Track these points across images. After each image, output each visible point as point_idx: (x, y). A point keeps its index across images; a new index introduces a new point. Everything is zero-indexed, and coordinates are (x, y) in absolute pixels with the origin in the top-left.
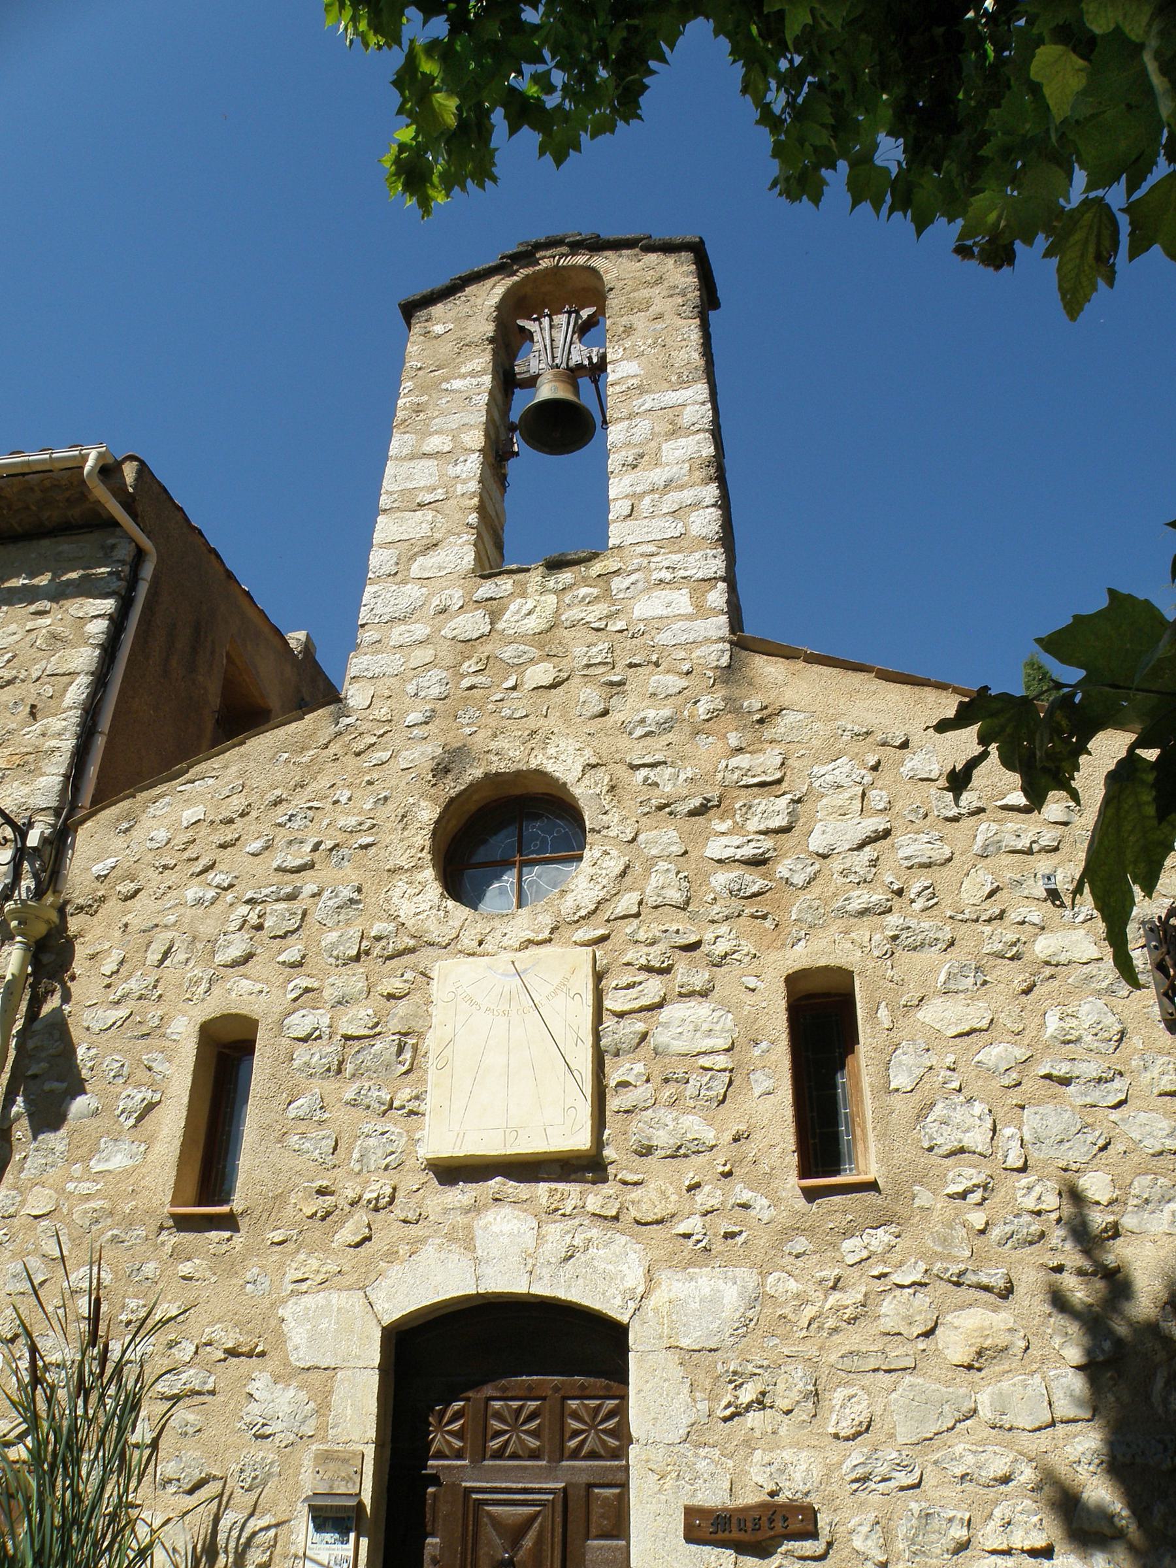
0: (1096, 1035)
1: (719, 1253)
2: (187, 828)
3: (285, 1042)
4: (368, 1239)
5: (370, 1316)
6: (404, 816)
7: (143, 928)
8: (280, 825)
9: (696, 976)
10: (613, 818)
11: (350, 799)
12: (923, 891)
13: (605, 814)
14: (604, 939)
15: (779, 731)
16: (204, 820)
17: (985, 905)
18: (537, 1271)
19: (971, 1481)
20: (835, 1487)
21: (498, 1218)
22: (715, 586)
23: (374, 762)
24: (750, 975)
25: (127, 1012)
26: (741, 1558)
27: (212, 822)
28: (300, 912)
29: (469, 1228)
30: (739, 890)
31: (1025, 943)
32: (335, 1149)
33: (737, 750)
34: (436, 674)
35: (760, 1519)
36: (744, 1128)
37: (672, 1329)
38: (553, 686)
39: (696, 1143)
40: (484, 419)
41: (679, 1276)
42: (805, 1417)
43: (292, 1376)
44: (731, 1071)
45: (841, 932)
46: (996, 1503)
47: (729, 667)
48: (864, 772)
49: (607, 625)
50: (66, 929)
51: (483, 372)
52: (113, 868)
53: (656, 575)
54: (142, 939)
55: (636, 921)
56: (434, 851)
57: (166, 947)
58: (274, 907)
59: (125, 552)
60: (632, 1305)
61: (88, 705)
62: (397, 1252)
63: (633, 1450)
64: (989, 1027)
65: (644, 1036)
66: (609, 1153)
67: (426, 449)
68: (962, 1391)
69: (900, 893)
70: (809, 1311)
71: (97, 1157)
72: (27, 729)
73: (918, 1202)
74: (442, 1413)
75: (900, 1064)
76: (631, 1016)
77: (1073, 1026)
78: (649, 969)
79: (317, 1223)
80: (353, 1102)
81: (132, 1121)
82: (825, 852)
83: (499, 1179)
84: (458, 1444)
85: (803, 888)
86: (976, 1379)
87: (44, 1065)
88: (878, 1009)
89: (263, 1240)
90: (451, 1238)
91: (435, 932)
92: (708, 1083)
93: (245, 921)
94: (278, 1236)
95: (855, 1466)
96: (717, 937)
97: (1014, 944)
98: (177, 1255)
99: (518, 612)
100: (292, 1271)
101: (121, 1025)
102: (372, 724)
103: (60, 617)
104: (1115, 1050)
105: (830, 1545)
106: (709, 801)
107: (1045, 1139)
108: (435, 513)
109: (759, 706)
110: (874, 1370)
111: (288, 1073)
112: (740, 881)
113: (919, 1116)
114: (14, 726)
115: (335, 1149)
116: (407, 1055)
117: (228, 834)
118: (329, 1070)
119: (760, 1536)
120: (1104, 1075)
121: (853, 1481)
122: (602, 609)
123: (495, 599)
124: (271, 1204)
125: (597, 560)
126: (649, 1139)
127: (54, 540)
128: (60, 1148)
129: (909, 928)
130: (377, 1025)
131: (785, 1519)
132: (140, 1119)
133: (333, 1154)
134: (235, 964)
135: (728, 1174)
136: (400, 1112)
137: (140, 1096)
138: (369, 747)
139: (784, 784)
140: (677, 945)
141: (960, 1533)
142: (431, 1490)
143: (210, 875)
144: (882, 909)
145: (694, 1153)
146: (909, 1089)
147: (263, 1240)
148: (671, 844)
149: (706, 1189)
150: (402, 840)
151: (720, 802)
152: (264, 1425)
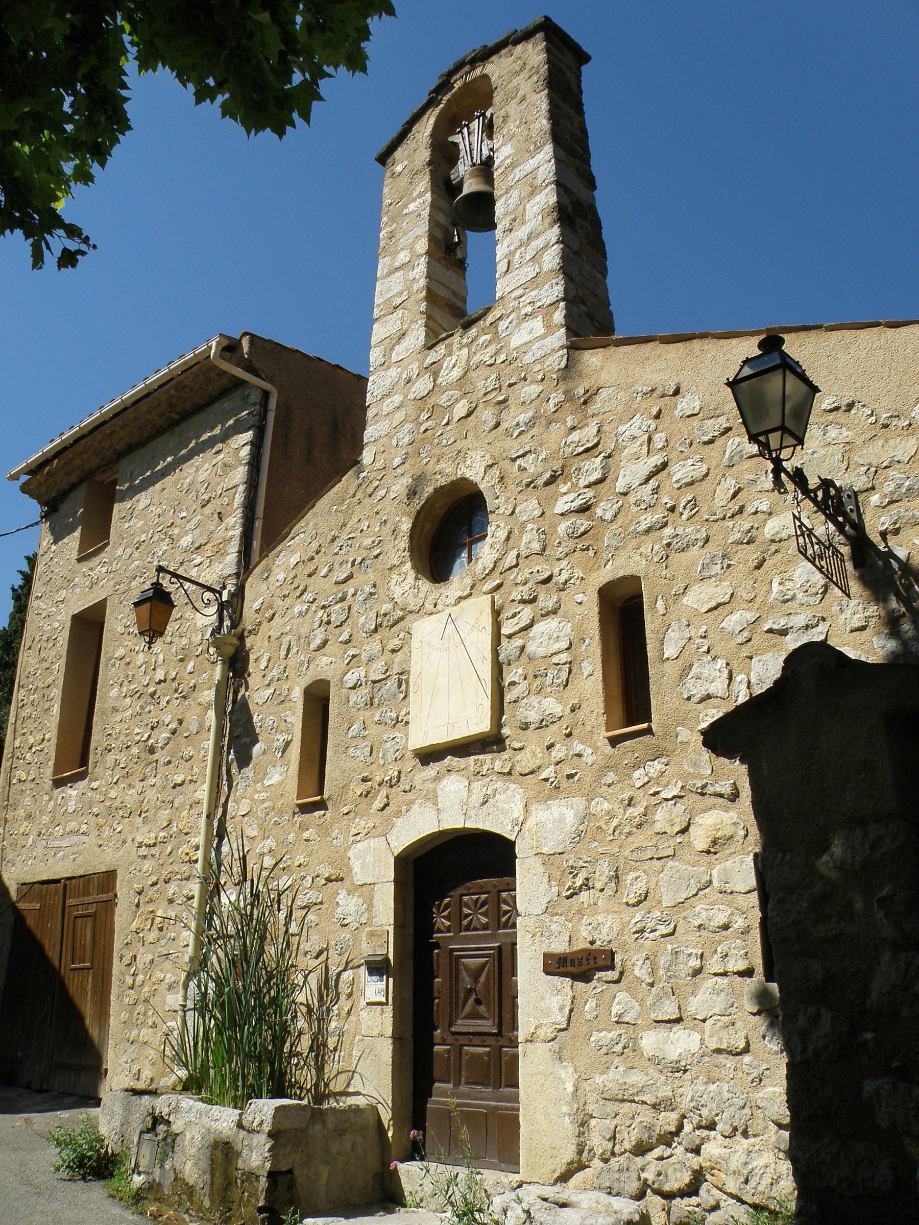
0: (807, 591)
1: (565, 789)
4: (387, 805)
5: (389, 851)
6: (394, 531)
8: (336, 554)
9: (546, 601)
10: (502, 500)
11: (368, 527)
12: (687, 504)
14: (499, 586)
18: (468, 814)
19: (704, 929)
20: (626, 937)
23: (378, 498)
26: (575, 983)
27: (304, 561)
29: (435, 790)
30: (573, 533)
31: (757, 528)
32: (371, 753)
34: (408, 426)
35: (582, 959)
36: (576, 702)
37: (538, 842)
38: (469, 415)
42: (611, 893)
43: (356, 890)
44: (570, 663)
46: (720, 942)
47: (566, 367)
48: (650, 422)
49: (495, 360)
51: (425, 192)
52: (262, 603)
53: (523, 312)
55: (517, 570)
56: (412, 549)
59: (255, 397)
60: (517, 829)
63: (519, 920)
65: (523, 648)
66: (506, 731)
67: (397, 264)
68: (702, 869)
69: (672, 509)
70: (615, 822)
73: (680, 739)
74: (439, 905)
75: (671, 639)
77: (790, 587)
78: (523, 602)
81: (280, 753)
83: (449, 757)
84: (448, 923)
85: (612, 521)
86: (713, 860)
87: (241, 729)
88: (656, 601)
95: (636, 923)
96: (561, 570)
97: (749, 531)
98: (303, 828)
99: (447, 368)
104: (821, 601)
105: (622, 973)
106: (556, 472)
107: (765, 679)
109: (582, 392)
110: (651, 859)
113: (682, 676)
114: (213, 528)
115: (371, 753)
116: (404, 687)
117: (311, 567)
118: (366, 704)
119: (582, 969)
120: (810, 622)
121: (634, 933)
122: (492, 348)
123: (435, 363)
126: (526, 718)
128: (251, 775)
129: (678, 535)
130: (387, 670)
131: (595, 958)
132: (284, 752)
134: (319, 648)
135: (569, 735)
137: (282, 738)
139: (600, 446)
141: (696, 963)
142: (436, 951)
144: (660, 525)
146: (675, 657)
148: (534, 510)
149: (557, 746)
150: (394, 547)
151: (563, 471)
152: (344, 919)
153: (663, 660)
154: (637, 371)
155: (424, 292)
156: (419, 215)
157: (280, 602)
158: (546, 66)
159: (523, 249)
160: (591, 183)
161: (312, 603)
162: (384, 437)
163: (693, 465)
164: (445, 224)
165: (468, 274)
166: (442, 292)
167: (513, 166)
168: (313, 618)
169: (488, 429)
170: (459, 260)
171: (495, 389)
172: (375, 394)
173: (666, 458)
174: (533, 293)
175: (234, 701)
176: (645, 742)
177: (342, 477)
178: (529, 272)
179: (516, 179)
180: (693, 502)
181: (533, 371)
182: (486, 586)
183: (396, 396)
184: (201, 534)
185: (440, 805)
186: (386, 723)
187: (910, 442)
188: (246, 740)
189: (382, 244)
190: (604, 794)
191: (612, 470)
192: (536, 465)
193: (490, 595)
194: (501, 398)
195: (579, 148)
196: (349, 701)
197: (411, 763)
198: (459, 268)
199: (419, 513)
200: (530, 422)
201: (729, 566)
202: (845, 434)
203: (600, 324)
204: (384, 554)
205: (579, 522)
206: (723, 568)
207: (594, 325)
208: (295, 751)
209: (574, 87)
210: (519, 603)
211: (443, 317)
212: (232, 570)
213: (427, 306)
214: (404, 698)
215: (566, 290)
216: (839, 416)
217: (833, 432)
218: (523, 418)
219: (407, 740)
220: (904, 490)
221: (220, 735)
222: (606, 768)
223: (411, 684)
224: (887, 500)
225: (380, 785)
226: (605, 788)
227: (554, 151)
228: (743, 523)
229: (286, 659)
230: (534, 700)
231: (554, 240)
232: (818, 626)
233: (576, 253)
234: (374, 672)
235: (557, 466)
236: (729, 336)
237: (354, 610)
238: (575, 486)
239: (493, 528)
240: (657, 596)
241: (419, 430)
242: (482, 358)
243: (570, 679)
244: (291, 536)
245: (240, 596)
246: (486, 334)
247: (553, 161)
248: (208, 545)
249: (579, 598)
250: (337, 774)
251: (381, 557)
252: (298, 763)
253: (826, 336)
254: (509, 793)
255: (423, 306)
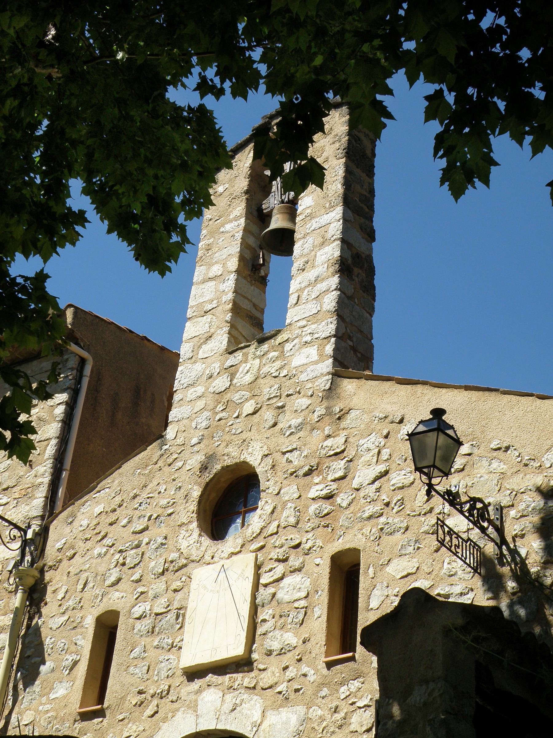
0: (464, 570)
1: (293, 700)
2: (96, 517)
3: (131, 621)
4: (156, 712)
6: (186, 496)
7: (76, 573)
8: (136, 509)
9: (295, 561)
10: (271, 483)
11: (165, 490)
12: (397, 502)
13: (268, 481)
14: (262, 547)
15: (347, 422)
16: (104, 512)
17: (425, 506)
18: (220, 717)
21: (208, 694)
22: (329, 341)
23: (176, 468)
24: (319, 558)
25: (68, 617)
27: (107, 512)
28: (141, 554)
29: (196, 701)
30: (319, 513)
32: (148, 671)
33: (328, 436)
34: (206, 414)
36: (307, 636)
38: (254, 413)
39: (288, 646)
40: (239, 249)
41: (275, 712)
44: (306, 608)
45: (359, 530)
47: (330, 389)
48: (381, 440)
49: (279, 374)
50: (44, 579)
52: (65, 544)
53: (305, 339)
54: (75, 579)
55: (277, 536)
56: (199, 512)
57: (85, 581)
58: (130, 553)
60: (255, 729)
61: (57, 456)
62: (167, 717)
64: (416, 572)
65: (274, 595)
66: (255, 656)
67: (211, 275)
69: (387, 504)
70: (325, 724)
71: (52, 692)
72: (28, 474)
75: (375, 595)
76: (270, 586)
78: (278, 560)
79: (137, 708)
80: (157, 647)
81: (68, 671)
82: (358, 487)
83: (210, 675)
85: (346, 508)
87: (33, 650)
88: (369, 568)
89: (115, 720)
90: (189, 707)
91: (195, 554)
92: (296, 615)
93: (118, 562)
94: (121, 717)
96: (308, 540)
100: (126, 733)
101: (65, 624)
102: (176, 447)
103: (42, 407)
104: (472, 577)
106: (313, 467)
108: (212, 316)
109: (338, 410)
111: (132, 636)
112: (319, 509)
114: (22, 473)
115: (148, 671)
116: (180, 619)
118: (148, 632)
120: (463, 591)
122: (278, 364)
123: (234, 366)
124: (119, 701)
125: (280, 334)
126: (271, 646)
127: (39, 360)
129: (388, 523)
130: (168, 606)
133: (147, 673)
135: (300, 660)
136: (176, 648)
137: (71, 658)
138: (174, 461)
139: (345, 452)
140: (291, 546)
143: (104, 541)
144: (378, 514)
145: (288, 651)
146: (376, 608)
147: (115, 720)
148: (294, 493)
149: (291, 668)
150: (185, 509)
151: (318, 467)
153: (368, 610)
154: (377, 401)
155: (231, 304)
156: (233, 236)
157: (81, 544)
158: (347, 138)
159: (311, 288)
160: (371, 236)
161: (111, 547)
162: (185, 419)
163: (405, 475)
164: (254, 245)
165: (267, 288)
166: (246, 305)
167: (311, 216)
168: (110, 559)
169: (268, 426)
170: (262, 277)
171: (276, 397)
172: (182, 382)
173: (388, 467)
174: (314, 326)
175: (28, 627)
176: (350, 666)
177: (147, 446)
178: (312, 308)
179: (312, 228)
180: (401, 501)
181: (306, 387)
182: (253, 546)
183: (199, 387)
184: (9, 477)
185: (199, 712)
186: (163, 648)
187: (539, 478)
188: (38, 659)
189: (200, 253)
190: (319, 704)
191: (352, 471)
192: (299, 460)
193: (255, 553)
194: (280, 404)
195: (365, 207)
196: (134, 629)
197: (180, 679)
198: (261, 283)
199: (207, 484)
200: (299, 426)
201: (419, 548)
202: (502, 467)
203: (362, 354)
204: (176, 513)
205: (324, 506)
206: (414, 549)
207: (357, 356)
208: (82, 669)
209: (369, 153)
210: (275, 561)
211: (245, 328)
212: (38, 512)
213: (232, 316)
214: (180, 628)
215: (337, 329)
216: (500, 453)
217: (495, 464)
218: (295, 422)
219: (179, 661)
220: (530, 509)
221: (12, 656)
222: (321, 685)
223: (187, 616)
224: (520, 514)
225: (152, 697)
226: (320, 699)
227: (343, 213)
228: (431, 519)
229: (82, 592)
230: (278, 633)
231: (334, 287)
232: (468, 594)
233: (350, 298)
234: (158, 606)
235: (314, 462)
236: (440, 386)
237: (146, 556)
238: (325, 479)
239: (263, 503)
240: (370, 565)
241: (215, 418)
242: (269, 369)
243: (305, 620)
244: (97, 489)
245: (42, 536)
246: (275, 351)
247: (341, 221)
248: (16, 488)
249: (318, 561)
250: (117, 687)
251: (173, 516)
252: (84, 678)
253: (501, 397)
254: (252, 702)
255: (228, 317)
